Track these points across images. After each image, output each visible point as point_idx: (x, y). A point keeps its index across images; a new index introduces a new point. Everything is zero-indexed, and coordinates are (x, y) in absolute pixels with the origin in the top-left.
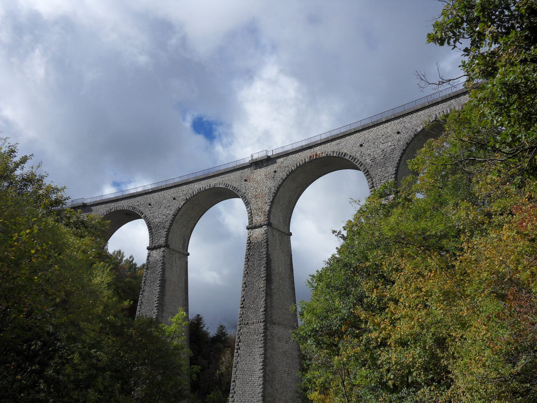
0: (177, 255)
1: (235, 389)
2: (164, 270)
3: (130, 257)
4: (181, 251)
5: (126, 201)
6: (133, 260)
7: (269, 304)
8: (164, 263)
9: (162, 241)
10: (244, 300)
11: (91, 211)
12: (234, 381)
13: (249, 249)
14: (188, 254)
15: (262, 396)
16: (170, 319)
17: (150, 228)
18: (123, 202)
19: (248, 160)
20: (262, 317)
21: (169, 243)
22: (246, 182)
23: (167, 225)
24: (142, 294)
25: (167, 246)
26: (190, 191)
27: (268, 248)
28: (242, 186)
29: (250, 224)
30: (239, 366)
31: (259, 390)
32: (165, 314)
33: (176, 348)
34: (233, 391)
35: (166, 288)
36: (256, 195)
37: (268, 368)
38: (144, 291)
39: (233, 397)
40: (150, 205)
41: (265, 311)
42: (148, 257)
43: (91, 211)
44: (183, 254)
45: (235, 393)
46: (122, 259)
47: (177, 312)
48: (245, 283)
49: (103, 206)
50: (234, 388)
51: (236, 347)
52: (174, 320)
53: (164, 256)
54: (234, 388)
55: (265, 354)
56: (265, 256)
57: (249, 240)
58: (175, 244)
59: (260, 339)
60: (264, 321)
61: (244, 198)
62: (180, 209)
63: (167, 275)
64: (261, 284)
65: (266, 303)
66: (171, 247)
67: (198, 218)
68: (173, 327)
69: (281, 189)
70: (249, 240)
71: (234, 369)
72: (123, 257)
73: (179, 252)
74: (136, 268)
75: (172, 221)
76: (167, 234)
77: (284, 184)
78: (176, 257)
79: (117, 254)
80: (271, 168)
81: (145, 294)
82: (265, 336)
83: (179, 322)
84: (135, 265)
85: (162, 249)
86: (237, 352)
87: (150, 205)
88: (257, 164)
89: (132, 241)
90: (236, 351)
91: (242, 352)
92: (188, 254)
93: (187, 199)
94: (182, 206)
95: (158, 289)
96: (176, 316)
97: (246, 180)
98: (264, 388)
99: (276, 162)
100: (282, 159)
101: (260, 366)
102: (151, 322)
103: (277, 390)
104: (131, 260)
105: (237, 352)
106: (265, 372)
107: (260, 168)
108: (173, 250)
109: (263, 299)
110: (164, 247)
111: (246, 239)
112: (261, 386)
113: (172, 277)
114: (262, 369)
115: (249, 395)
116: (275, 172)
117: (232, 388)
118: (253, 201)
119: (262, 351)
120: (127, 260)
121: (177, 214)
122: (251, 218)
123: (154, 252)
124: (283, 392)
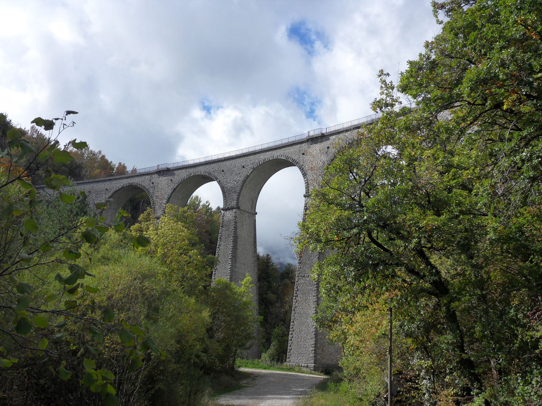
0: (247, 215)
2: (236, 228)
3: (207, 202)
4: (250, 211)
5: (203, 167)
6: (209, 205)
8: (236, 223)
9: (234, 203)
11: (174, 174)
12: (293, 322)
14: (256, 213)
15: (315, 334)
16: (240, 282)
17: (223, 188)
18: (200, 167)
19: (305, 137)
21: (240, 205)
22: (304, 156)
23: (238, 189)
24: (219, 248)
25: (238, 208)
26: (257, 161)
28: (301, 159)
29: (306, 193)
30: (297, 310)
32: (237, 265)
33: (245, 304)
36: (312, 168)
38: (220, 245)
39: (292, 334)
40: (223, 171)
43: (174, 174)
45: (293, 331)
46: (199, 204)
47: (244, 276)
49: (184, 171)
51: (295, 295)
52: (243, 283)
53: (236, 217)
57: (306, 206)
58: (245, 205)
59: (314, 289)
61: (301, 169)
62: (248, 177)
63: (238, 232)
66: (241, 208)
68: (243, 289)
71: (293, 312)
72: (200, 202)
74: (211, 212)
79: (195, 199)
81: (221, 247)
83: (247, 285)
84: (211, 209)
85: (234, 210)
86: (296, 299)
87: (223, 171)
88: (313, 140)
89: (210, 195)
90: (294, 298)
92: (256, 213)
95: (231, 244)
96: (245, 280)
97: (303, 154)
99: (329, 139)
100: (334, 137)
102: (227, 287)
104: (207, 204)
105: (296, 299)
107: (316, 143)
108: (243, 211)
109: (317, 257)
110: (236, 208)
111: (303, 205)
113: (243, 233)
116: (328, 148)
117: (291, 327)
118: (309, 173)
120: (204, 205)
121: (246, 180)
122: (307, 187)
123: (228, 212)
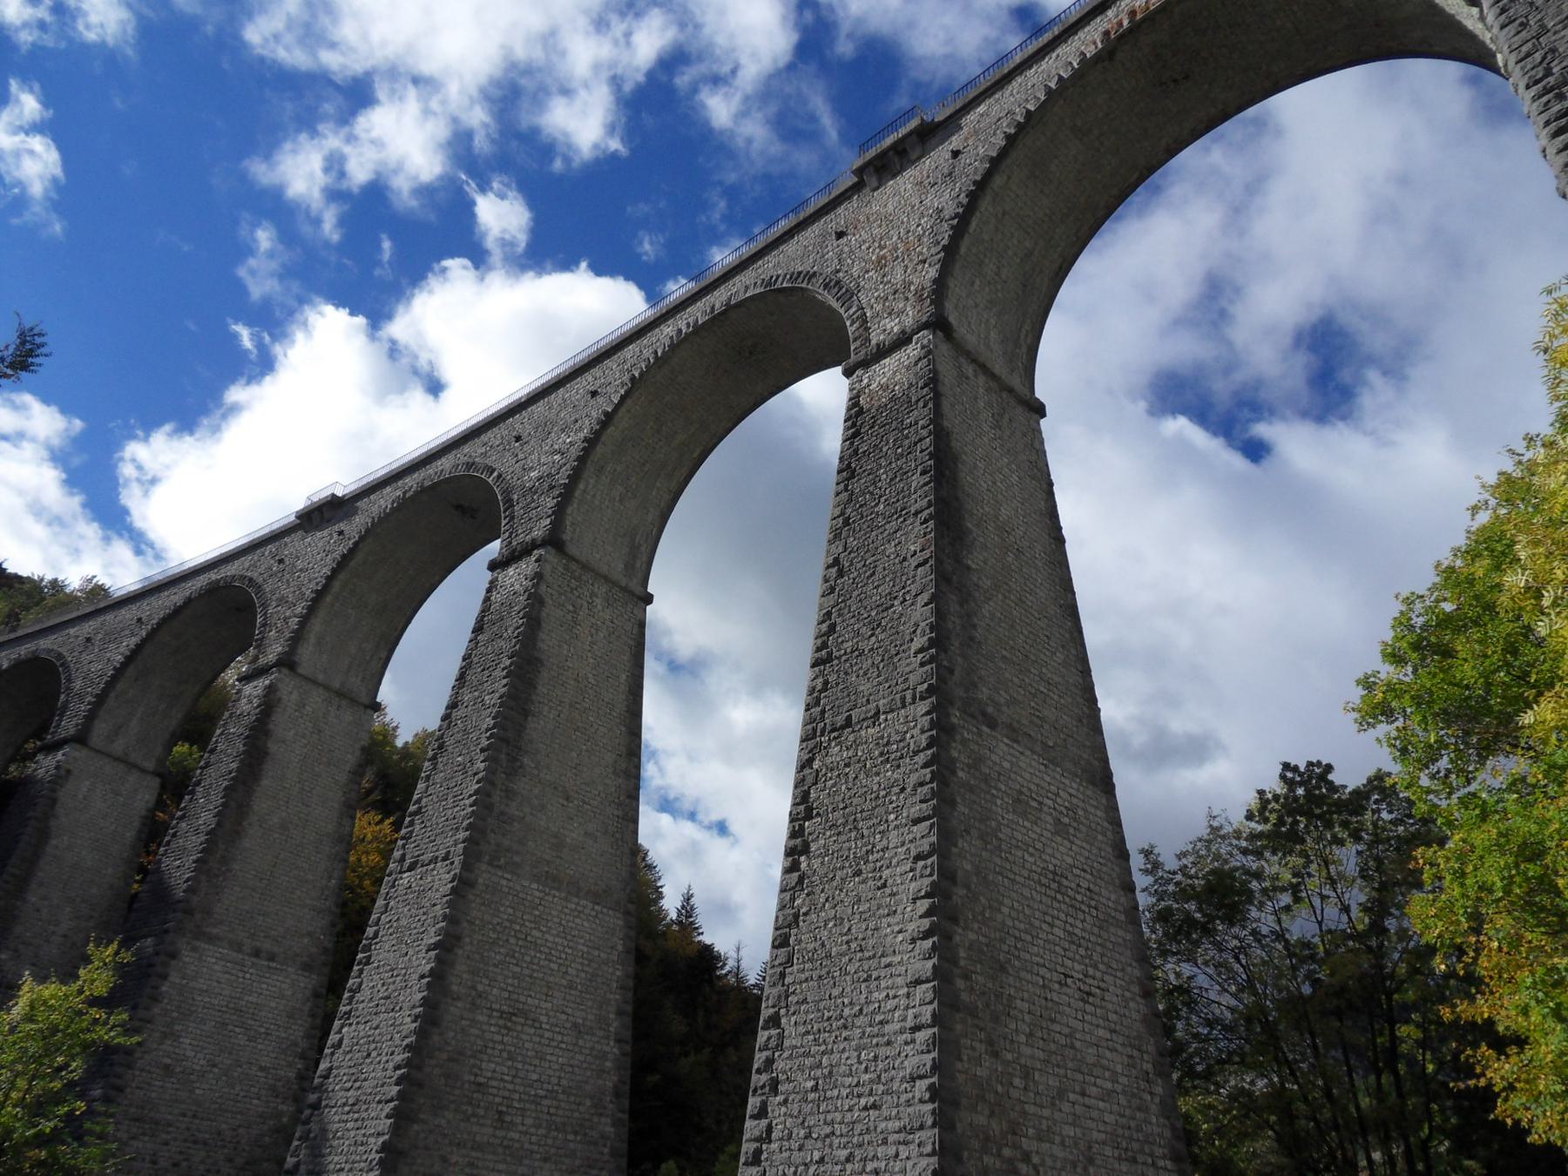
0: (602, 589)
1: (780, 1065)
7: (954, 623)
10: (832, 629)
12: (775, 1021)
13: (854, 436)
20: (914, 670)
27: (937, 406)
31: (916, 1057)
34: (764, 1077)
35: (541, 689)
37: (964, 937)
39: (762, 1113)
41: (932, 643)
42: (489, 591)
44: (625, 589)
45: (774, 1086)
48: (836, 562)
50: (770, 1062)
54: (770, 1062)
55: (943, 850)
56: (924, 433)
58: (593, 540)
60: (931, 691)
62: (607, 419)
63: (548, 641)
64: (915, 539)
65: (940, 614)
67: (685, 471)
69: (985, 204)
70: (856, 404)
73: (606, 579)
75: (579, 459)
76: (558, 504)
77: (998, 181)
78: (593, 595)
80: (939, 157)
82: (942, 769)
87: (518, 439)
91: (816, 863)
92: (649, 599)
93: (633, 379)
94: (617, 407)
98: (947, 1047)
101: (914, 916)
103: (1027, 1074)
106: (945, 952)
108: (585, 567)
112: (922, 1036)
114: (926, 935)
115: (855, 1093)
117: (759, 1058)
119: (923, 837)
124: (1061, 1094)
